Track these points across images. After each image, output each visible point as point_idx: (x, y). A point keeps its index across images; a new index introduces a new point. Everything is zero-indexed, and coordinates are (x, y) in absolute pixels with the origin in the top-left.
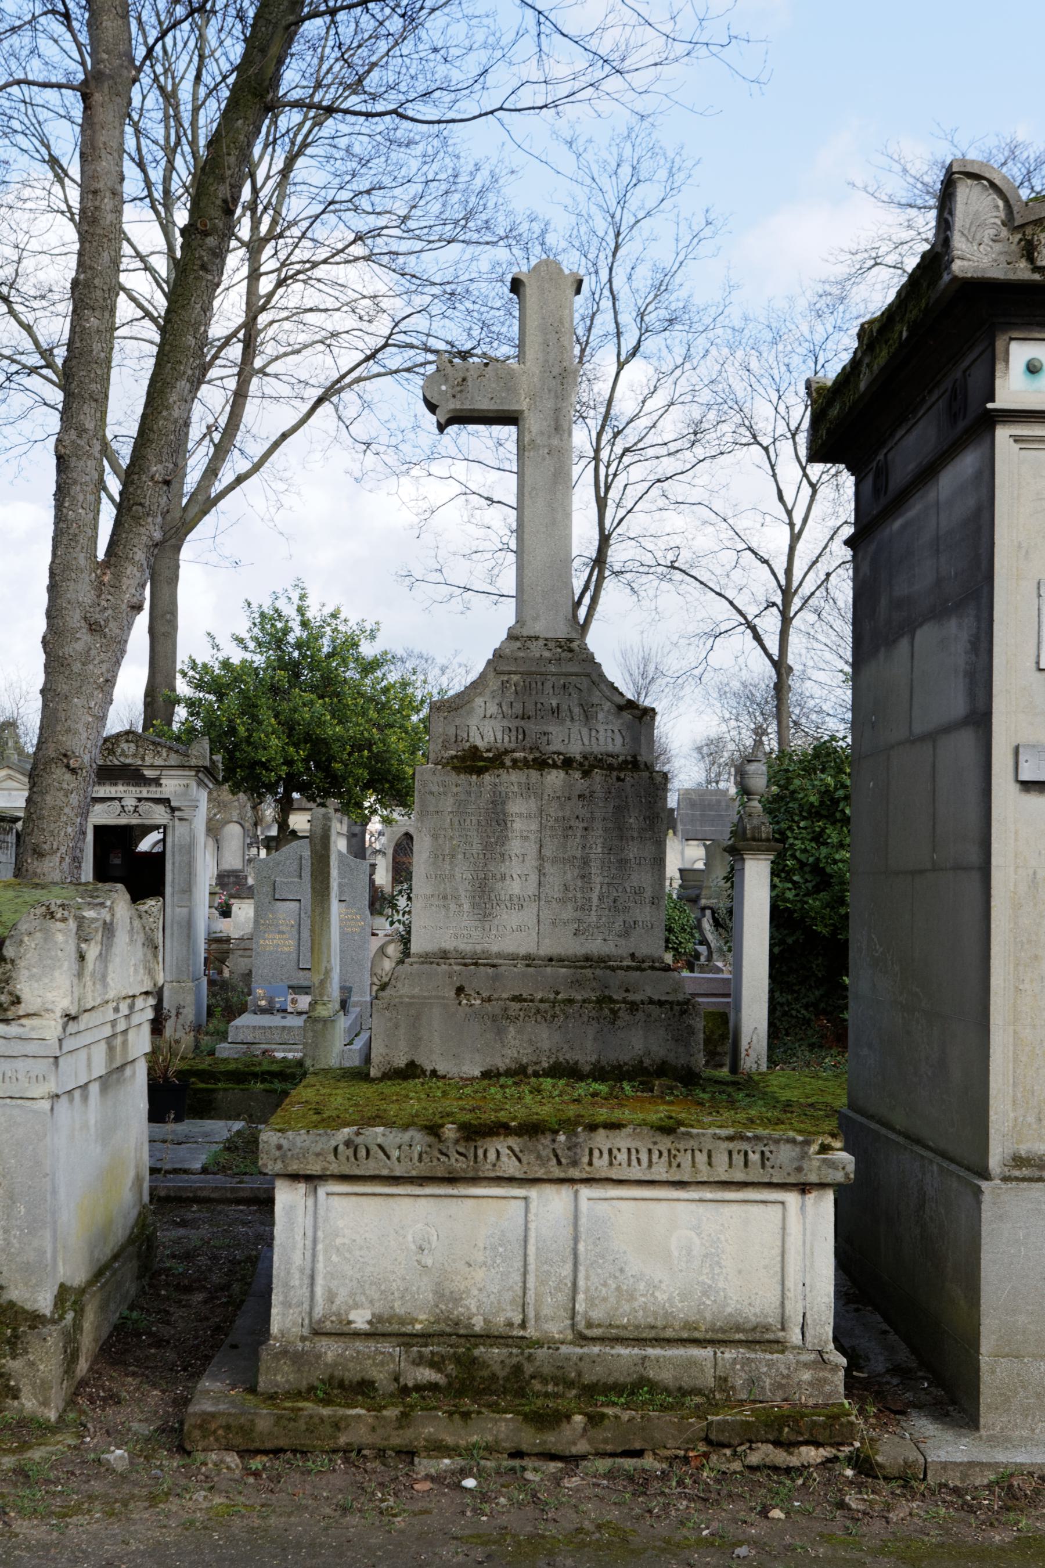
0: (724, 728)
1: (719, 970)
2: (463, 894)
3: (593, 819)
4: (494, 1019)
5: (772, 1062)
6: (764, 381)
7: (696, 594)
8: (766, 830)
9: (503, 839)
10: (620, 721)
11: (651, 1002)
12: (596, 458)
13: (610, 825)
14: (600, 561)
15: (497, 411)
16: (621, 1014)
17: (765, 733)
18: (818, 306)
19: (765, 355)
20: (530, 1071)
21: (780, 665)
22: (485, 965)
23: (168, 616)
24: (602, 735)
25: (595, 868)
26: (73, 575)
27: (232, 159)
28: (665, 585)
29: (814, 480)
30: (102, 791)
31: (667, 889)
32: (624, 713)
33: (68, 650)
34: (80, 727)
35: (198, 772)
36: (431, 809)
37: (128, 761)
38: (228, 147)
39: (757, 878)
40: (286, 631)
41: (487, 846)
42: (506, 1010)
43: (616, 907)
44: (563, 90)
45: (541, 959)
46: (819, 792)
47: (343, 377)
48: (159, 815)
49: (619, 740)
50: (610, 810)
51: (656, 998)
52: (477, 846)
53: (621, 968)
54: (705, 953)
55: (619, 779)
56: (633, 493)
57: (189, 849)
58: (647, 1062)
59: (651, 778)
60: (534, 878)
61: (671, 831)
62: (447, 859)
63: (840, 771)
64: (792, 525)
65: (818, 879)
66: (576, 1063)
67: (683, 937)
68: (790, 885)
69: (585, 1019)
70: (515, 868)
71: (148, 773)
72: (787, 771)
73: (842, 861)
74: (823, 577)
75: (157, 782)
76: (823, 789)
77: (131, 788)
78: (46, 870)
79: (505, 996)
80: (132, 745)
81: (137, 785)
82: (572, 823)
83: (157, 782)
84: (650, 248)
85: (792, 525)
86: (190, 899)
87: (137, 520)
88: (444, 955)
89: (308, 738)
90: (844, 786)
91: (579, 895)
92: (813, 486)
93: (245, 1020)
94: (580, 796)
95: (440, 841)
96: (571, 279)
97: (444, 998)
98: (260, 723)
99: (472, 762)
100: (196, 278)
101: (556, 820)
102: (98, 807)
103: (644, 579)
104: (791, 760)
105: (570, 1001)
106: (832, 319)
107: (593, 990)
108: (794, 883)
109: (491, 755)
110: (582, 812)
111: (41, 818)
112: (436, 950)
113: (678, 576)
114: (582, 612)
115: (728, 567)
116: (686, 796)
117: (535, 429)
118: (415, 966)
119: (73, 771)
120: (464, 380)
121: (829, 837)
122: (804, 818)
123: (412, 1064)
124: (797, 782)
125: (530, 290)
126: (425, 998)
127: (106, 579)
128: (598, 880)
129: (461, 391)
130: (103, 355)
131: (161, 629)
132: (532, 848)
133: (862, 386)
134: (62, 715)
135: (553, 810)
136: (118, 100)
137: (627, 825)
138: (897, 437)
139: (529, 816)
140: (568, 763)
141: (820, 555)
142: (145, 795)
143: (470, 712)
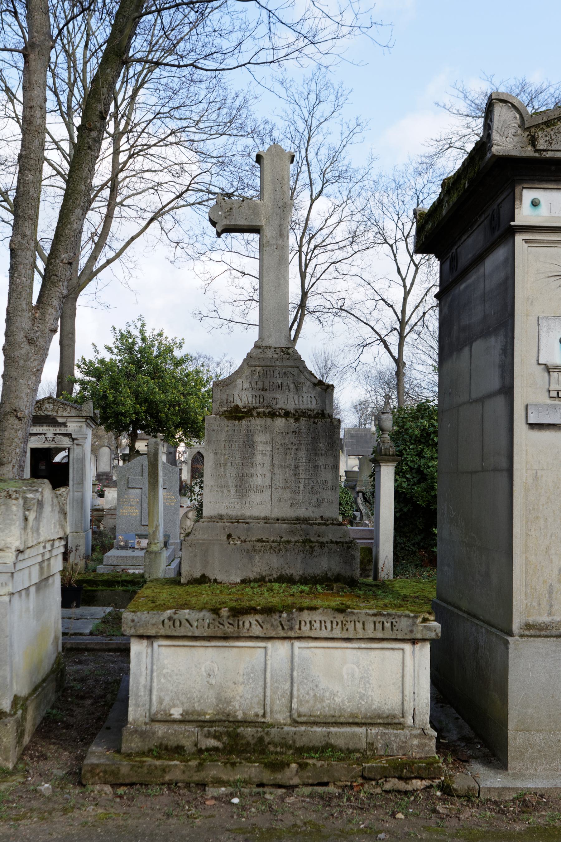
1: (367, 525)
2: (231, 484)
3: (300, 444)
4: (248, 551)
7: (354, 323)
8: (393, 450)
9: (252, 455)
10: (315, 392)
11: (332, 542)
13: (310, 447)
14: (302, 306)
16: (316, 548)
17: (390, 398)
19: (391, 196)
20: (267, 579)
21: (399, 362)
22: (243, 523)
23: (70, 336)
25: (301, 470)
27: (105, 90)
28: (337, 319)
30: (35, 430)
32: (317, 388)
33: (17, 354)
34: (23, 395)
35: (87, 419)
36: (214, 439)
37: (49, 413)
38: (102, 83)
40: (134, 343)
42: (254, 546)
43: (312, 491)
48: (66, 442)
49: (314, 402)
50: (310, 439)
51: (334, 540)
52: (238, 458)
53: (315, 524)
54: (359, 516)
55: (314, 423)
56: (320, 269)
57: (82, 461)
58: (330, 574)
59: (332, 422)
60: (269, 476)
62: (222, 466)
63: (431, 418)
64: (405, 286)
65: (420, 476)
66: (292, 575)
67: (347, 507)
68: (405, 480)
69: (297, 551)
70: (259, 470)
71: (60, 420)
73: (433, 467)
74: (422, 314)
75: (64, 425)
76: (422, 428)
77: (51, 428)
79: (253, 539)
80: (51, 405)
81: (54, 426)
82: (289, 446)
83: (64, 425)
84: (327, 138)
85: (405, 286)
87: (54, 283)
88: (221, 517)
90: (434, 426)
94: (293, 432)
95: (219, 456)
96: (288, 155)
97: (220, 540)
99: (236, 414)
101: (281, 444)
102: (33, 438)
103: (326, 315)
105: (289, 542)
106: (426, 176)
107: (301, 536)
108: (407, 478)
110: (294, 440)
113: (344, 314)
114: (293, 333)
115: (371, 309)
117: (269, 236)
118: (205, 523)
119: (20, 419)
120: (231, 209)
122: (412, 444)
123: (203, 576)
124: (409, 424)
125: (266, 161)
127: (37, 315)
130: (35, 195)
131: (66, 342)
132: (268, 460)
133: (444, 212)
134: (14, 389)
135: (279, 439)
140: (287, 414)
142: (58, 432)
143: (235, 386)
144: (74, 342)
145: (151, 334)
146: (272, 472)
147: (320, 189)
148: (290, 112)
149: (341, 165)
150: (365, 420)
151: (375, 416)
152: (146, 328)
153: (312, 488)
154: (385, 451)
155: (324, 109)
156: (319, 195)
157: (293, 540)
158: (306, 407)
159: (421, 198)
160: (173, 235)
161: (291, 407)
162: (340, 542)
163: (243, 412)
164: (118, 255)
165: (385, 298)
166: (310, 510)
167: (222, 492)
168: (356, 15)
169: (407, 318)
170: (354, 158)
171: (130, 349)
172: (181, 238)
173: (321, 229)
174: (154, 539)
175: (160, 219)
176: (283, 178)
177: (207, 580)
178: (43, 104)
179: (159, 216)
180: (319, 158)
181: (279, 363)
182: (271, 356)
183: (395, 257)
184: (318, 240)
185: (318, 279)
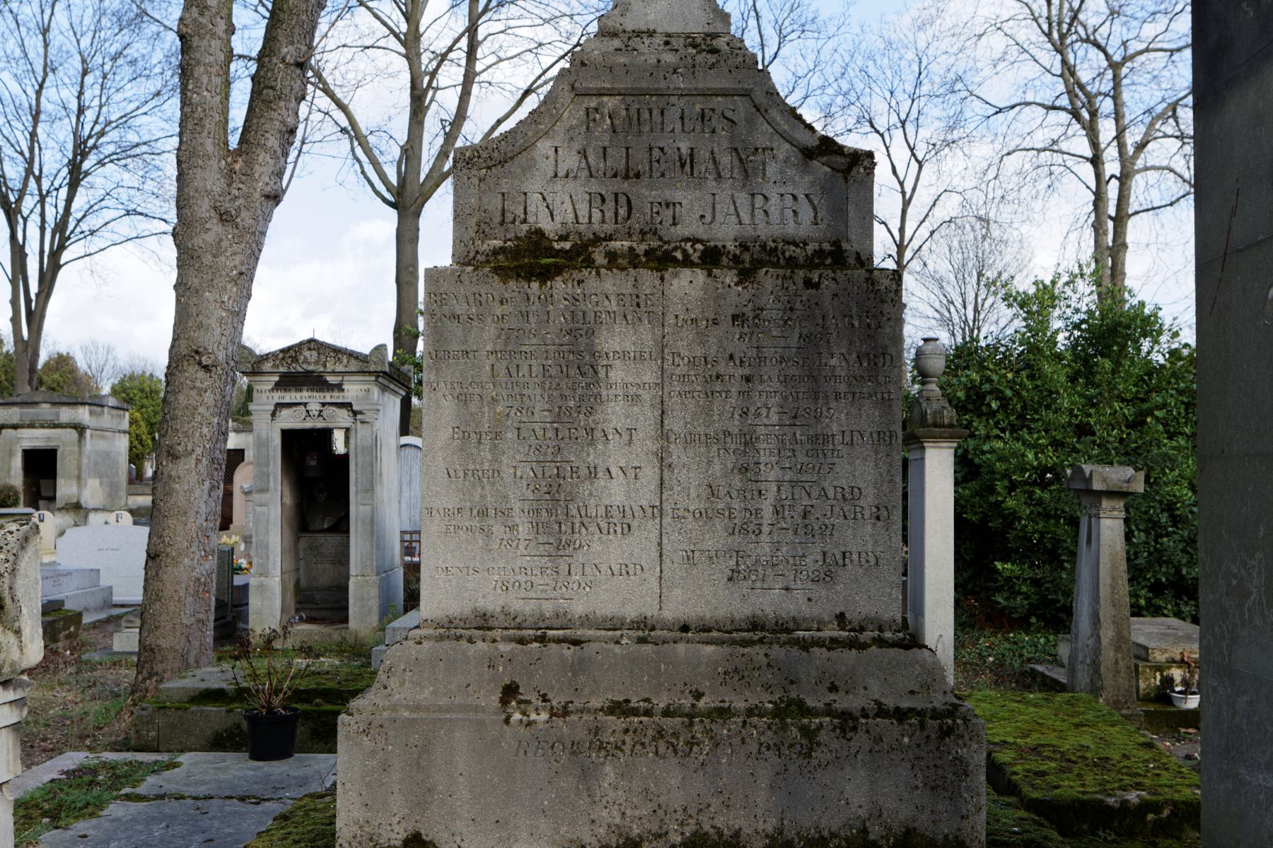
2: (517, 506)
3: (761, 359)
4: (575, 749)
9: (590, 402)
10: (808, 179)
11: (882, 712)
13: (794, 371)
16: (823, 736)
19: (879, 62)
22: (559, 641)
24: (774, 205)
25: (766, 454)
26: (200, 162)
30: (290, 397)
33: (198, 241)
34: (213, 322)
36: (455, 346)
37: (311, 368)
39: (939, 467)
41: (560, 416)
42: (597, 731)
43: (807, 526)
48: (343, 417)
49: (806, 214)
50: (794, 341)
51: (890, 703)
53: (819, 643)
55: (808, 284)
57: (373, 448)
58: (875, 832)
59: (871, 280)
60: (650, 473)
62: (486, 440)
64: (903, 193)
65: (966, 470)
66: (737, 834)
69: (754, 748)
70: (614, 455)
71: (331, 379)
75: (339, 387)
77: (315, 394)
78: (181, 473)
79: (596, 703)
80: (314, 353)
81: (321, 390)
82: (721, 368)
83: (339, 387)
85: (903, 193)
86: (372, 498)
88: (483, 622)
90: (989, 380)
91: (736, 505)
95: (473, 407)
97: (476, 709)
101: (692, 362)
105: (723, 713)
107: (768, 687)
109: (567, 245)
110: (740, 347)
111: (174, 418)
112: (467, 612)
118: (426, 645)
119: (206, 368)
121: (977, 429)
126: (440, 709)
127: (237, 167)
131: (405, 279)
132: (646, 417)
134: (194, 310)
135: (685, 344)
137: (827, 372)
139: (640, 357)
140: (711, 258)
142: (328, 400)
143: (531, 165)
146: (662, 460)
154: (934, 417)
157: (740, 705)
158: (776, 231)
159: (924, 63)
161: (725, 233)
162: (911, 710)
163: (558, 253)
166: (799, 594)
167: (486, 532)
181: (680, 83)
182: (653, 61)
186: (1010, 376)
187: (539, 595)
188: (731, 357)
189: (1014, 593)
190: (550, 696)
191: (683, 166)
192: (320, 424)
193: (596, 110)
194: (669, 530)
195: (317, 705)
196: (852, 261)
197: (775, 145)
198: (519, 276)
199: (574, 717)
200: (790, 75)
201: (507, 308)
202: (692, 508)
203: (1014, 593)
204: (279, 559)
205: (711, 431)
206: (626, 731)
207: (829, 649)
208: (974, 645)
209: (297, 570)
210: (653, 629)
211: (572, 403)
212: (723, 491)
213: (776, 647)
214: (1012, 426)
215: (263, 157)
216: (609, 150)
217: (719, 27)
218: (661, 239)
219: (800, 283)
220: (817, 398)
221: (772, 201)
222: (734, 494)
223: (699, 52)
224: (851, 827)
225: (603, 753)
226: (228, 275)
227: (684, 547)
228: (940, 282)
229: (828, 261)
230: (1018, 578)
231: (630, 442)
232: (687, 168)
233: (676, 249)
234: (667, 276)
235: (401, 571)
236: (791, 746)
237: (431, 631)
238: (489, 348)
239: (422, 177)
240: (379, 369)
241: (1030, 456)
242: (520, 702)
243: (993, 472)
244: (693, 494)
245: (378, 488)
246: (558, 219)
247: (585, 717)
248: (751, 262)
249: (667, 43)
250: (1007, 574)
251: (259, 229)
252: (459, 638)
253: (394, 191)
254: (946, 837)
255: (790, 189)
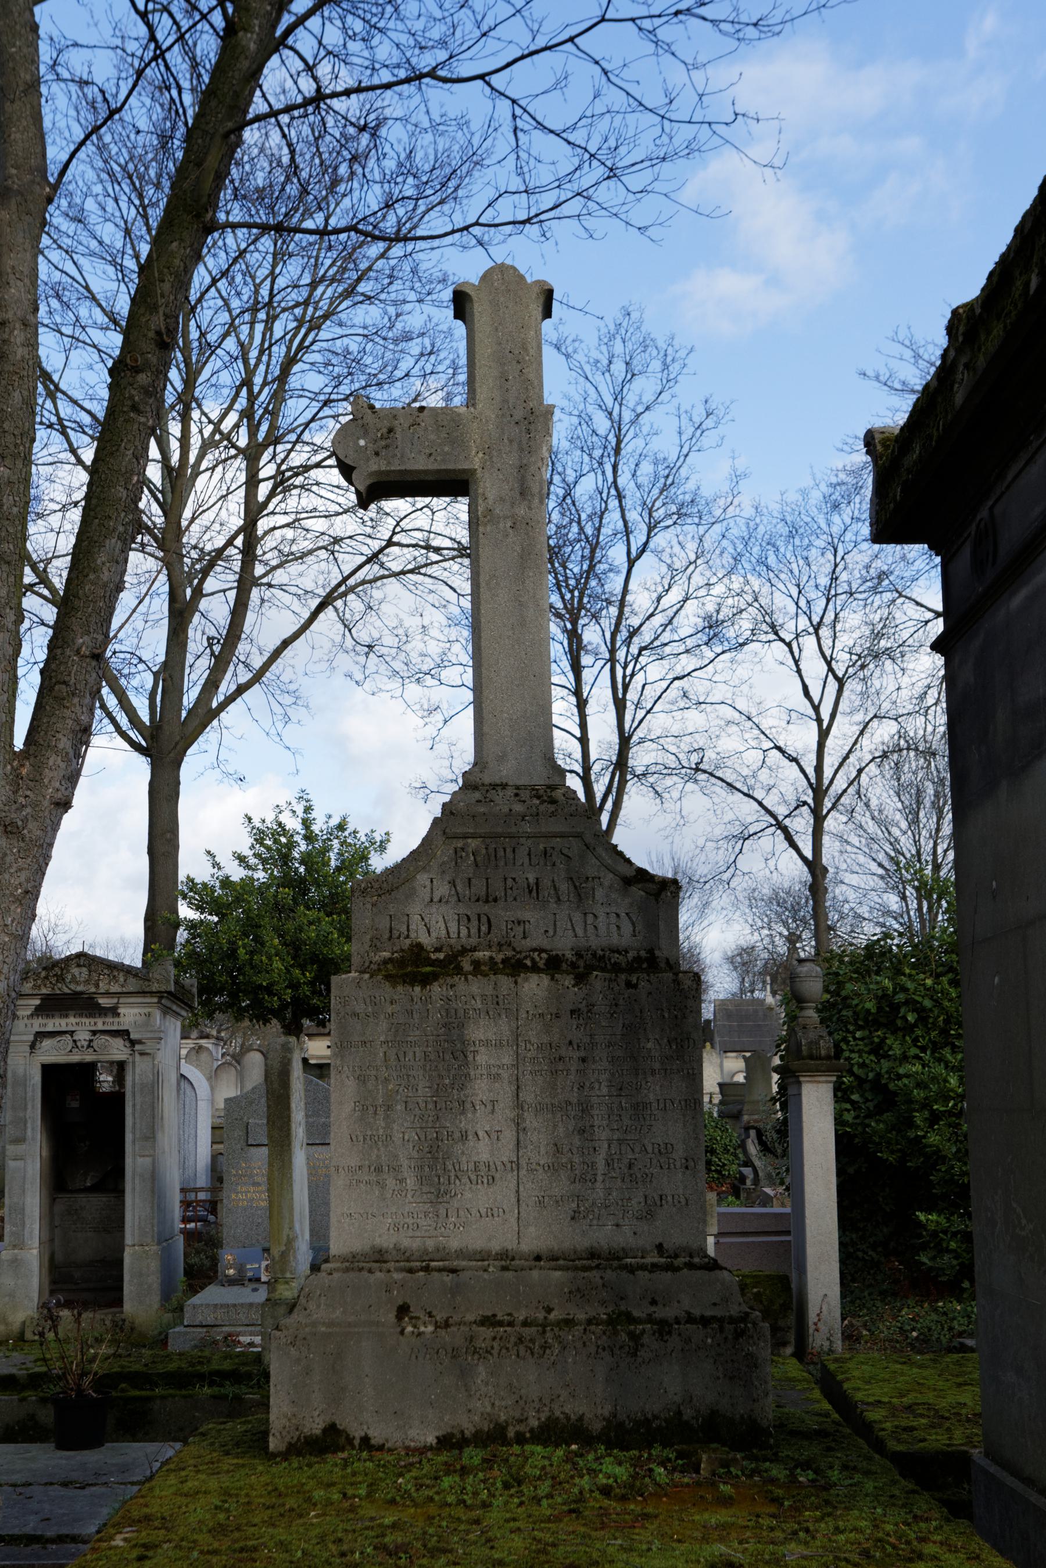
0: (756, 936)
1: (767, 1200)
2: (406, 1164)
5: (850, 1336)
6: (782, 576)
7: (724, 794)
8: (826, 1046)
9: (462, 1080)
10: (627, 901)
11: (690, 1319)
12: (612, 660)
14: (621, 764)
15: (438, 471)
16: (645, 1339)
17: (799, 938)
18: (833, 497)
19: (782, 550)
20: (511, 1433)
21: (815, 866)
22: (440, 1270)
23: (168, 835)
25: (599, 1117)
27: (167, 286)
28: (690, 786)
29: (840, 675)
30: (52, 1024)
31: (706, 1107)
32: (634, 889)
35: (161, 998)
37: (80, 988)
38: (161, 272)
40: (291, 845)
44: (547, 200)
45: (523, 1257)
46: (876, 997)
47: (345, 579)
48: (118, 1050)
49: (627, 928)
51: (697, 1312)
52: (423, 1089)
53: (643, 1267)
54: (751, 1176)
55: (629, 985)
56: (651, 693)
58: (688, 1413)
59: (677, 982)
60: (509, 1135)
61: (708, 1044)
62: (381, 1111)
63: (899, 972)
64: (819, 720)
66: (581, 1418)
67: (726, 1158)
68: (848, 1106)
70: (481, 1122)
71: (103, 1001)
72: (837, 974)
73: (907, 1076)
74: (854, 774)
75: (114, 1011)
76: (880, 993)
77: (84, 1020)
79: (470, 1317)
80: (84, 970)
81: (91, 1015)
82: (563, 1052)
83: (114, 1011)
84: (657, 437)
85: (819, 720)
86: (153, 1147)
87: (60, 700)
88: (379, 1257)
89: (314, 958)
90: (905, 990)
91: (577, 1159)
92: (841, 682)
93: (212, 1294)
94: (572, 1012)
95: (370, 1085)
96: (536, 290)
98: (263, 944)
99: (415, 967)
100: (126, 421)
102: (47, 1043)
103: (669, 781)
104: (841, 962)
105: (568, 1323)
106: (849, 510)
107: (603, 1303)
108: (853, 1103)
112: (367, 1249)
113: (702, 777)
114: (605, 818)
115: (755, 767)
116: (722, 1006)
117: (491, 495)
118: (336, 1275)
120: (390, 430)
121: (890, 1048)
122: (860, 1028)
123: (332, 1429)
124: (849, 986)
125: (479, 309)
127: (24, 771)
128: (604, 1135)
129: (387, 447)
130: (15, 510)
132: (504, 1092)
133: (959, 398)
136: (28, 219)
138: (1010, 478)
139: (499, 1045)
140: (554, 965)
141: (850, 751)
144: (176, 847)
145: (324, 827)
147: (644, 539)
148: (578, 399)
149: (682, 493)
150: (753, 983)
151: (771, 975)
152: (314, 814)
153: (630, 1166)
155: (643, 388)
156: (643, 551)
157: (581, 1316)
160: (363, 634)
161: (564, 944)
162: (713, 1317)
164: (258, 677)
165: (781, 744)
168: (701, 96)
169: (826, 782)
170: (705, 475)
171: (284, 857)
172: (376, 635)
173: (652, 615)
174: (283, 1271)
175: (339, 603)
176: (526, 350)
177: (342, 1440)
178: (30, 317)
179: (336, 599)
180: (640, 480)
181: (528, 828)
182: (506, 810)
183: (797, 666)
184: (646, 636)
185: (648, 712)
186: (929, 982)
187: (423, 1234)
188: (570, 1043)
189: (941, 1250)
190: (434, 1313)
191: (530, 892)
192: (89, 1058)
193: (463, 849)
194: (525, 1180)
195: (123, 1390)
196: (663, 965)
197: (602, 875)
198: (404, 982)
199: (454, 1329)
200: (664, 569)
201: (395, 1008)
202: (542, 1162)
203: (941, 1250)
204: (37, 1226)
205: (556, 1102)
206: (494, 1339)
207: (650, 1272)
208: (895, 1317)
209: (52, 1240)
210: (513, 1259)
211: (447, 1081)
212: (566, 1149)
213: (609, 1271)
214: (934, 1043)
215: (53, 760)
216: (473, 881)
217: (556, 780)
218: (514, 949)
219: (623, 985)
220: (637, 1074)
221: (600, 919)
222: (575, 1151)
223: (542, 803)
224: (669, 1410)
225: (476, 1356)
226: (12, 894)
227: (536, 1193)
228: (883, 823)
229: (645, 965)
230: (945, 1232)
231: (493, 1111)
232: (534, 894)
233: (526, 957)
234: (519, 980)
235: (180, 1240)
236: (621, 1348)
237: (338, 1265)
238: (382, 1039)
239: (184, 714)
240: (163, 988)
241: (953, 1081)
242: (411, 1318)
243: (910, 1101)
244: (543, 1151)
245: (159, 1135)
246: (434, 935)
247: (462, 1328)
248: (585, 967)
249: (517, 795)
250: (932, 1227)
251: (48, 840)
252: (361, 1269)
253: (147, 734)
254: (742, 1416)
255: (614, 909)
